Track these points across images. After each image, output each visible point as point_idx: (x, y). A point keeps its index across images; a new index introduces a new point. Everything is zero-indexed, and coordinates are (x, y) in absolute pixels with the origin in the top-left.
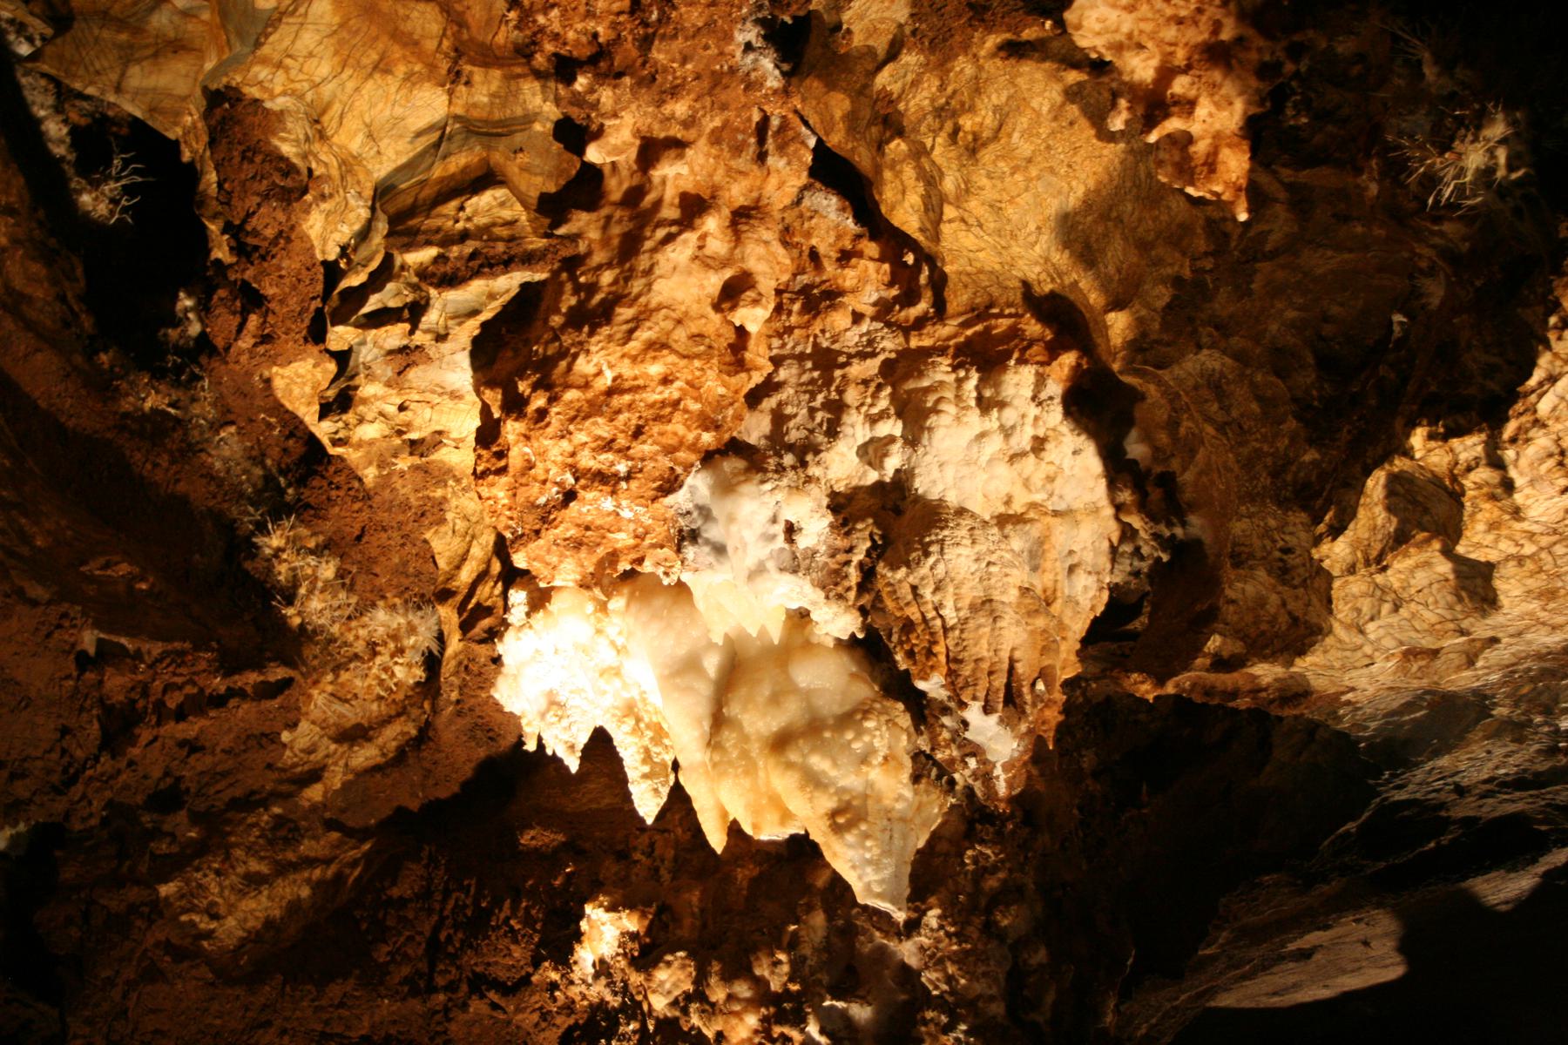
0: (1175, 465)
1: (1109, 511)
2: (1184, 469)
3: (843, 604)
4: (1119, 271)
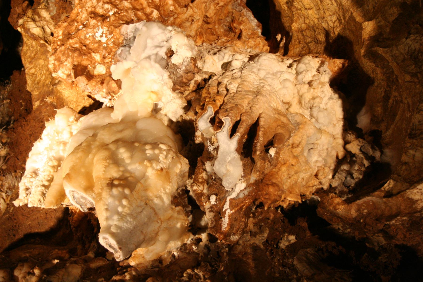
0: (383, 127)
1: (340, 141)
2: (387, 130)
3: (180, 95)
4: (374, 8)
